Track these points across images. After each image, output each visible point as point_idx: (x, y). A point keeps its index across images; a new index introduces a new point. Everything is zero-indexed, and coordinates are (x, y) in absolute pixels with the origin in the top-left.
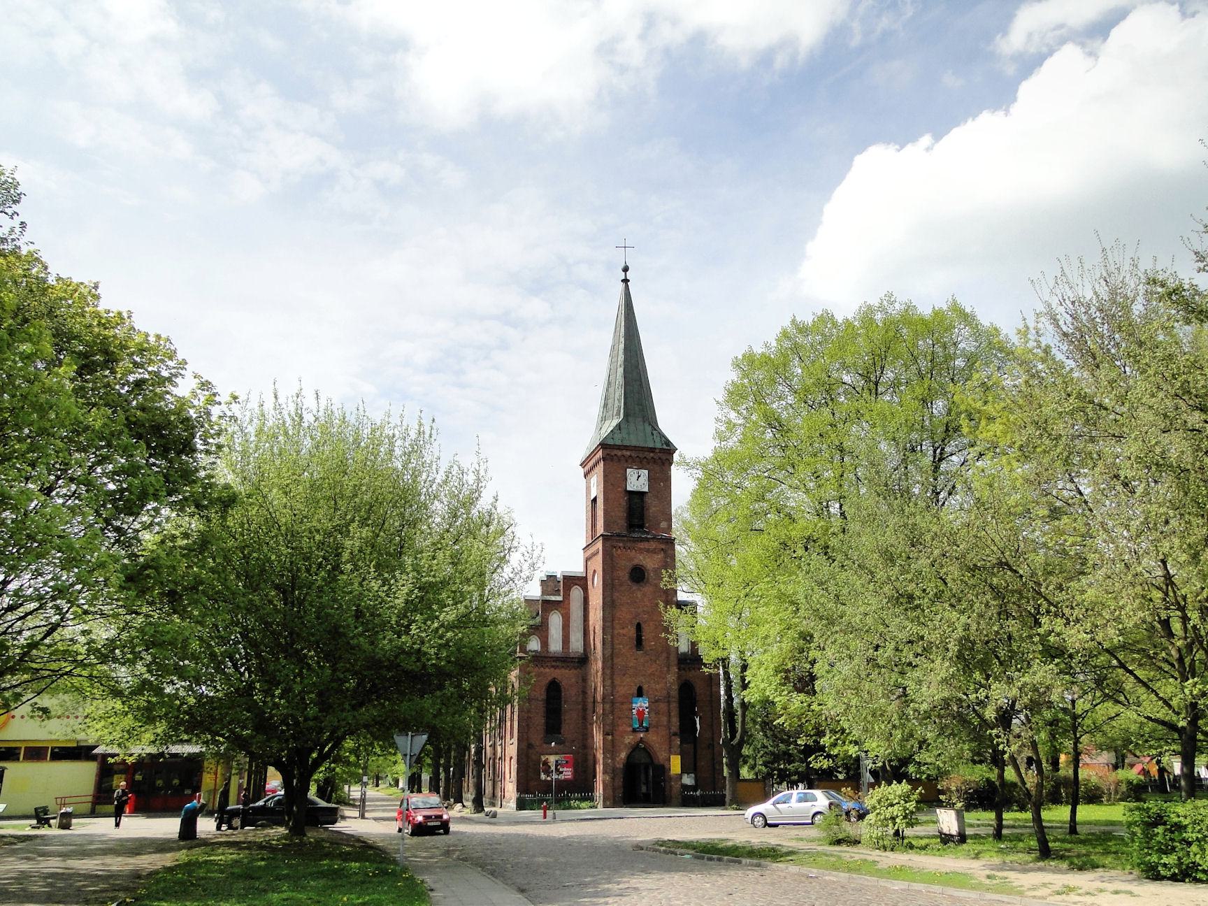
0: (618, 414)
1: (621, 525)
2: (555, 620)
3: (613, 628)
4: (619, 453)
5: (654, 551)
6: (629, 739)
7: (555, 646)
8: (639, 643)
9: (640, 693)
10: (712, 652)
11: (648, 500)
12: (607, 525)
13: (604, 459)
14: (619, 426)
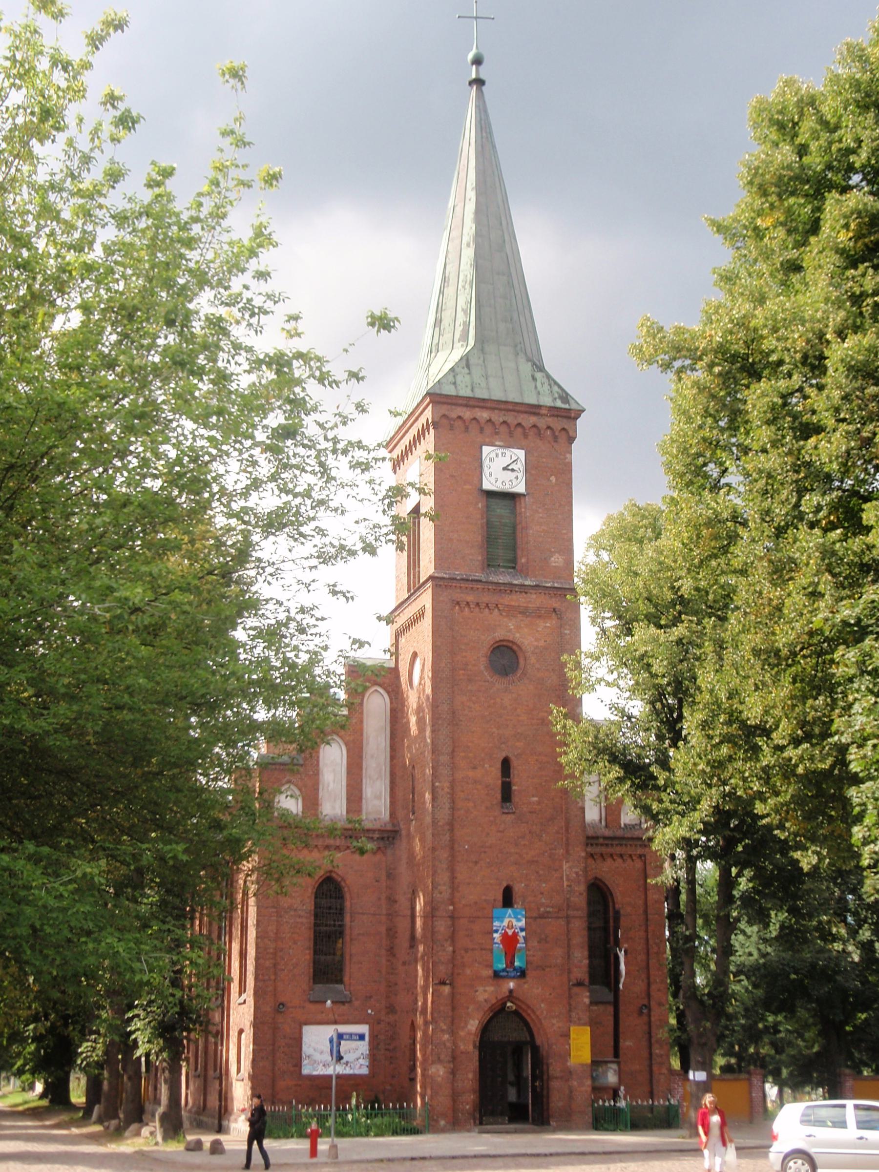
0: (465, 337)
1: (471, 565)
2: (333, 758)
3: (453, 767)
4: (467, 414)
5: (538, 614)
6: (487, 994)
7: (333, 806)
8: (507, 794)
9: (508, 900)
10: (693, 742)
11: (526, 509)
12: (440, 559)
13: (436, 425)
14: (466, 361)
